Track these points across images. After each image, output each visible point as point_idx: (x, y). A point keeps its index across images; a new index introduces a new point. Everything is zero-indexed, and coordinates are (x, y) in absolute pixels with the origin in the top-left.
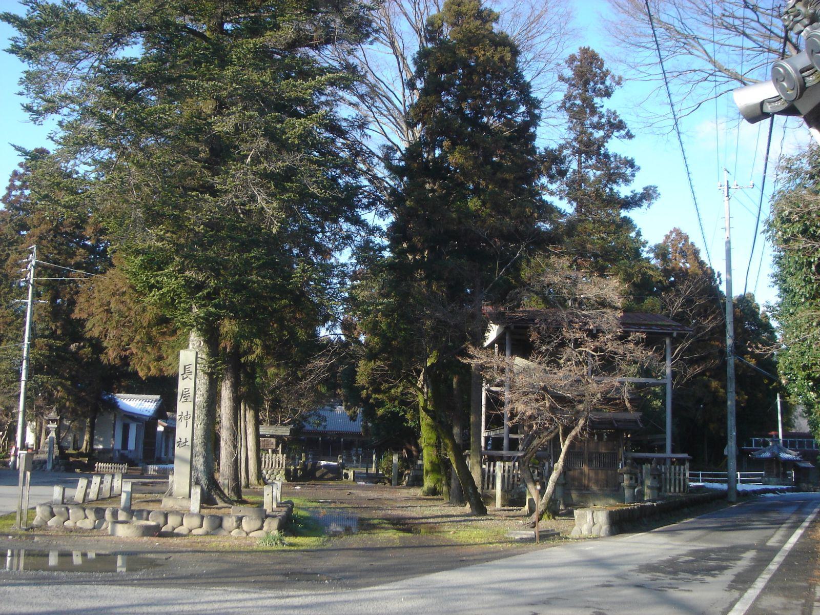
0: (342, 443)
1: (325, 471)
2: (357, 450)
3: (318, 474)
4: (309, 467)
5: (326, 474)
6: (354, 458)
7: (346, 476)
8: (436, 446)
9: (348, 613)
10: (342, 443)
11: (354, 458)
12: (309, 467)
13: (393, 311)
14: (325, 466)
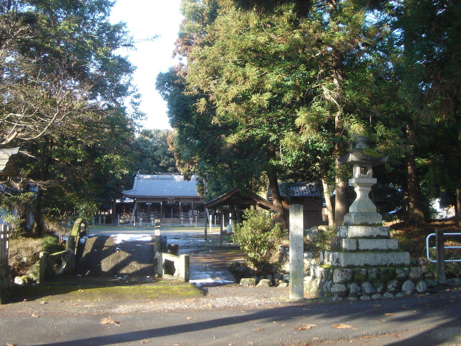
0: (161, 206)
1: (124, 255)
2: (193, 213)
3: (106, 265)
4: (88, 249)
5: (125, 263)
6: (191, 219)
7: (170, 268)
8: (218, 7)
9: (224, 345)
10: (161, 206)
11: (191, 219)
12: (88, 249)
13: (201, 146)
14: (125, 246)
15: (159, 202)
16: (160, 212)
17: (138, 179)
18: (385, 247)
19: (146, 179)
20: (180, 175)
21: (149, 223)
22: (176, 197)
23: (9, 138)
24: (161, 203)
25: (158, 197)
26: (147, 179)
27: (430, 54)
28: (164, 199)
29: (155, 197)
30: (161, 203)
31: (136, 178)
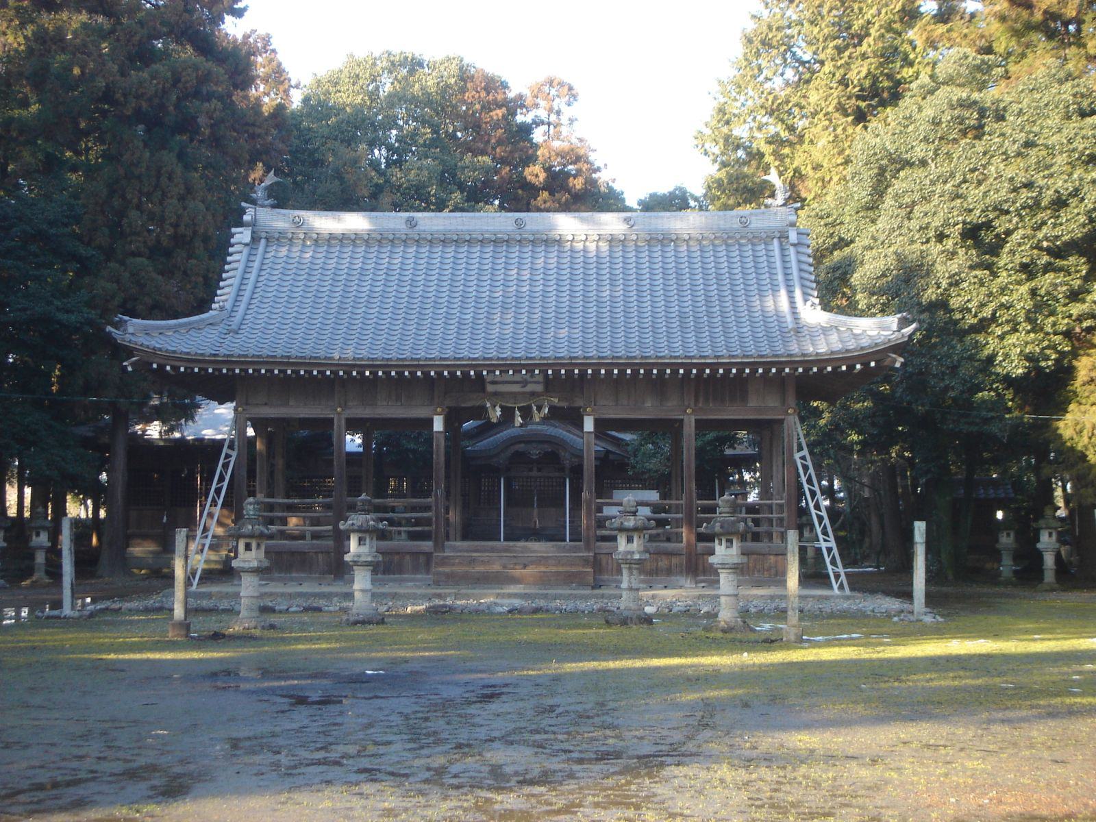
0: (439, 446)
15: (420, 412)
16: (428, 494)
17: (255, 239)
18: (251, 734)
19: (332, 237)
20: (516, 773)
21: (337, 588)
22: (556, 366)
23: (597, 805)
24: (438, 425)
25: (413, 367)
26: (344, 240)
27: (1003, 473)
28: (460, 386)
29: (387, 367)
30: (438, 425)
31: (242, 235)
